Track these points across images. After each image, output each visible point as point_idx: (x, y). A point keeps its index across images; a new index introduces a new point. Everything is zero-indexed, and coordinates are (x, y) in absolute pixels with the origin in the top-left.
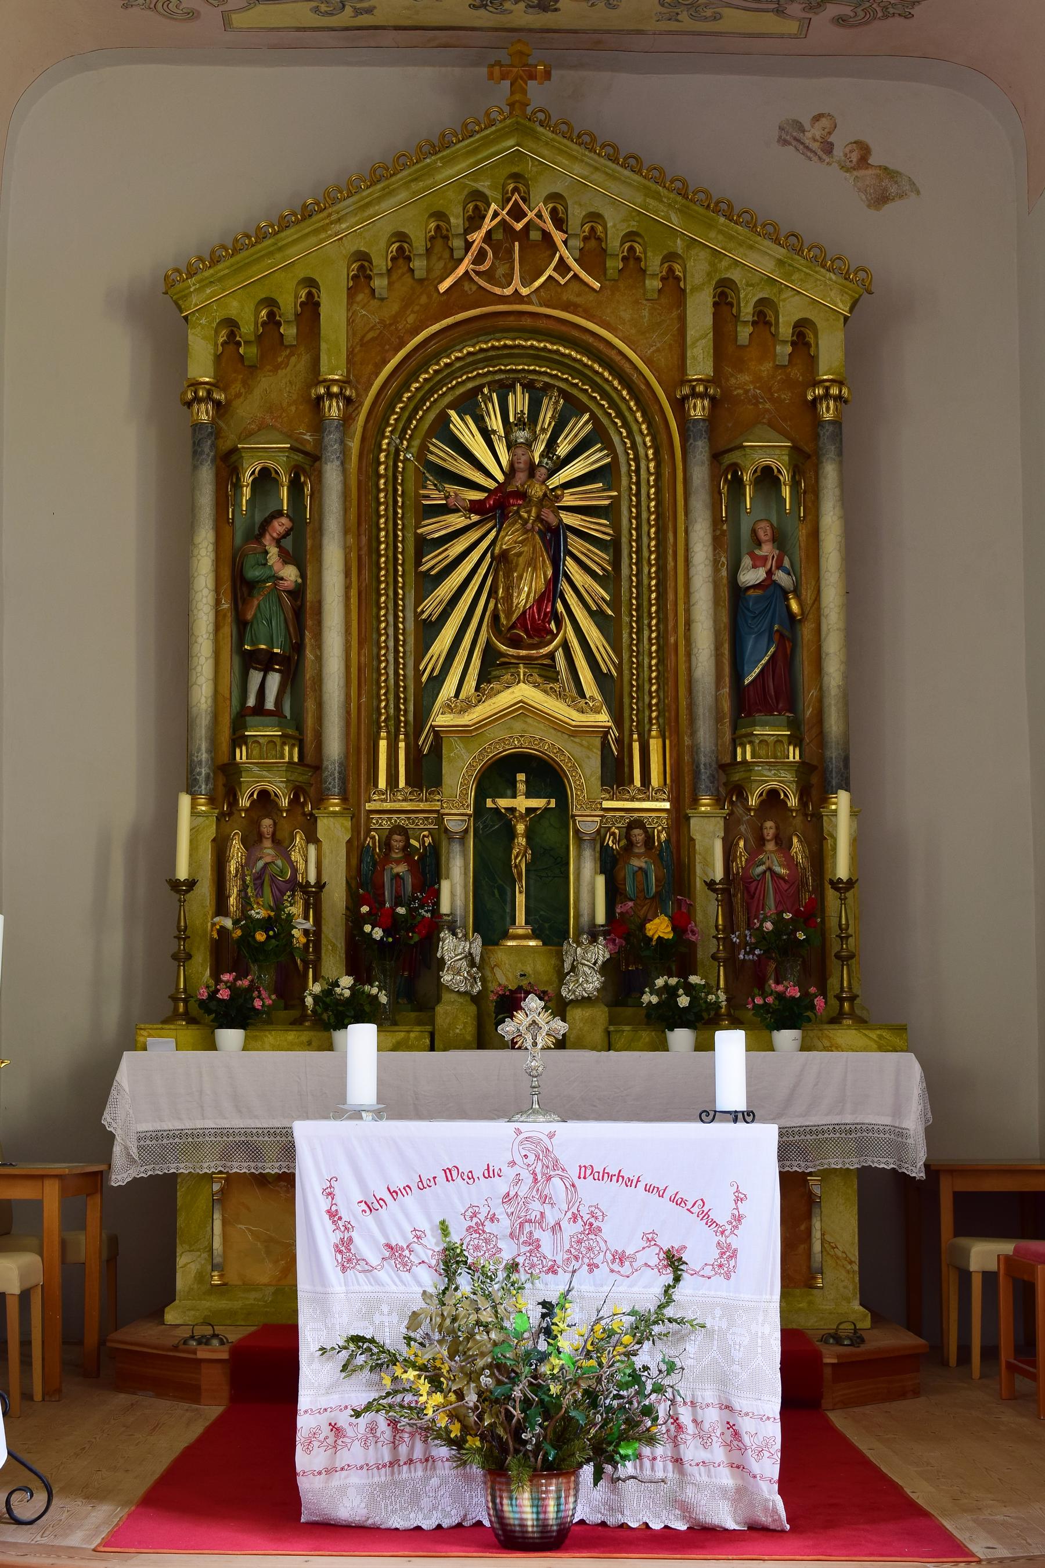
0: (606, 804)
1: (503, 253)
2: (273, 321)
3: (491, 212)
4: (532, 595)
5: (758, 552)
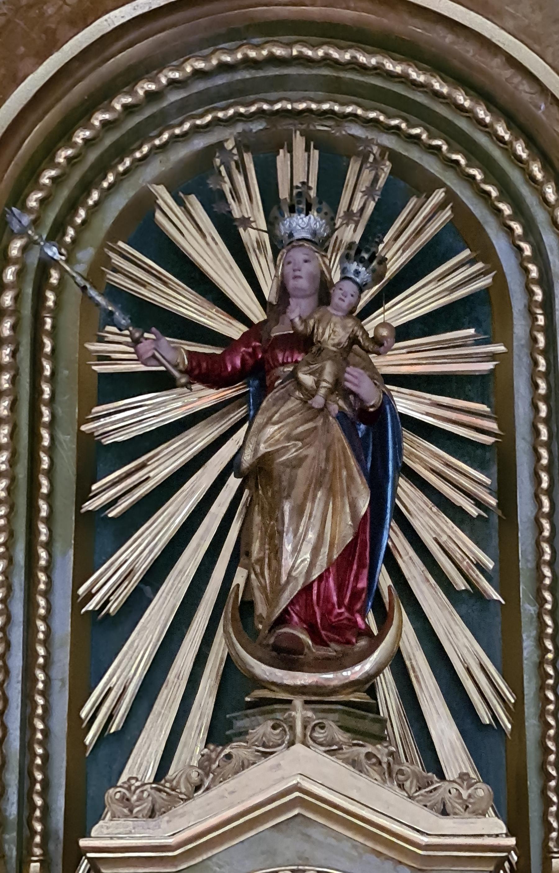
4: (325, 550)
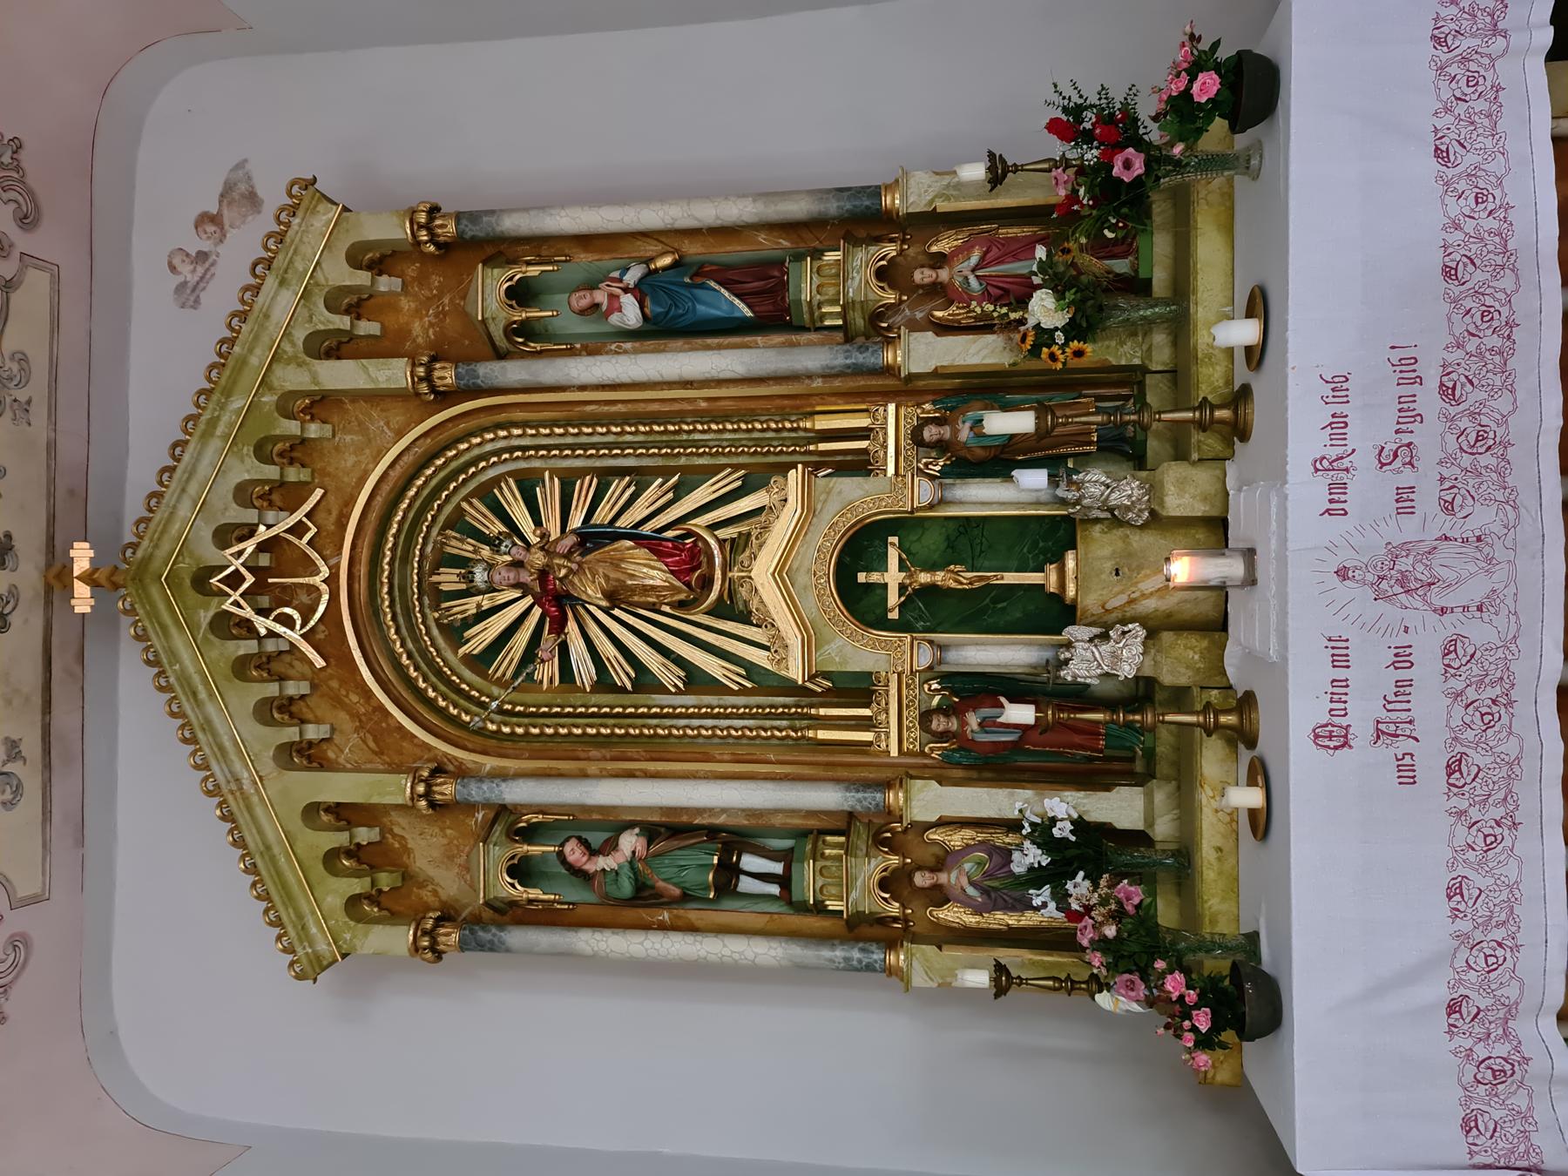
0: (891, 470)
1: (285, 596)
2: (355, 852)
3: (234, 610)
5: (604, 308)
